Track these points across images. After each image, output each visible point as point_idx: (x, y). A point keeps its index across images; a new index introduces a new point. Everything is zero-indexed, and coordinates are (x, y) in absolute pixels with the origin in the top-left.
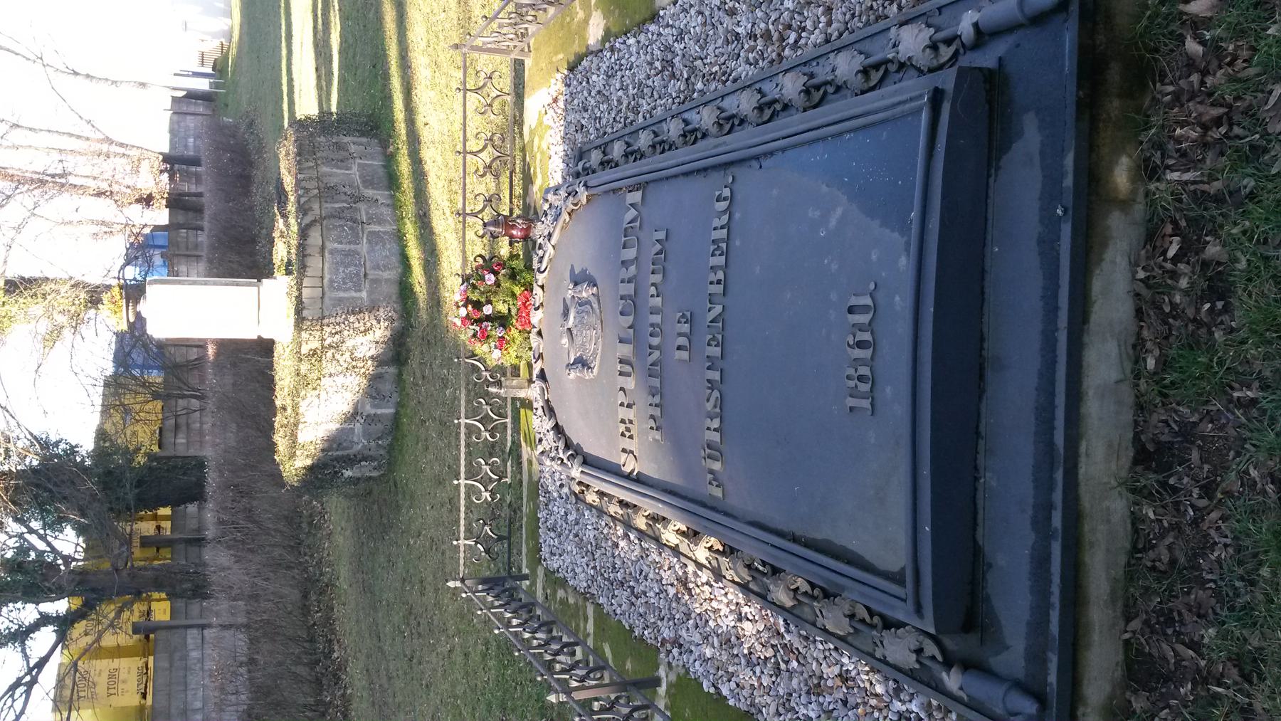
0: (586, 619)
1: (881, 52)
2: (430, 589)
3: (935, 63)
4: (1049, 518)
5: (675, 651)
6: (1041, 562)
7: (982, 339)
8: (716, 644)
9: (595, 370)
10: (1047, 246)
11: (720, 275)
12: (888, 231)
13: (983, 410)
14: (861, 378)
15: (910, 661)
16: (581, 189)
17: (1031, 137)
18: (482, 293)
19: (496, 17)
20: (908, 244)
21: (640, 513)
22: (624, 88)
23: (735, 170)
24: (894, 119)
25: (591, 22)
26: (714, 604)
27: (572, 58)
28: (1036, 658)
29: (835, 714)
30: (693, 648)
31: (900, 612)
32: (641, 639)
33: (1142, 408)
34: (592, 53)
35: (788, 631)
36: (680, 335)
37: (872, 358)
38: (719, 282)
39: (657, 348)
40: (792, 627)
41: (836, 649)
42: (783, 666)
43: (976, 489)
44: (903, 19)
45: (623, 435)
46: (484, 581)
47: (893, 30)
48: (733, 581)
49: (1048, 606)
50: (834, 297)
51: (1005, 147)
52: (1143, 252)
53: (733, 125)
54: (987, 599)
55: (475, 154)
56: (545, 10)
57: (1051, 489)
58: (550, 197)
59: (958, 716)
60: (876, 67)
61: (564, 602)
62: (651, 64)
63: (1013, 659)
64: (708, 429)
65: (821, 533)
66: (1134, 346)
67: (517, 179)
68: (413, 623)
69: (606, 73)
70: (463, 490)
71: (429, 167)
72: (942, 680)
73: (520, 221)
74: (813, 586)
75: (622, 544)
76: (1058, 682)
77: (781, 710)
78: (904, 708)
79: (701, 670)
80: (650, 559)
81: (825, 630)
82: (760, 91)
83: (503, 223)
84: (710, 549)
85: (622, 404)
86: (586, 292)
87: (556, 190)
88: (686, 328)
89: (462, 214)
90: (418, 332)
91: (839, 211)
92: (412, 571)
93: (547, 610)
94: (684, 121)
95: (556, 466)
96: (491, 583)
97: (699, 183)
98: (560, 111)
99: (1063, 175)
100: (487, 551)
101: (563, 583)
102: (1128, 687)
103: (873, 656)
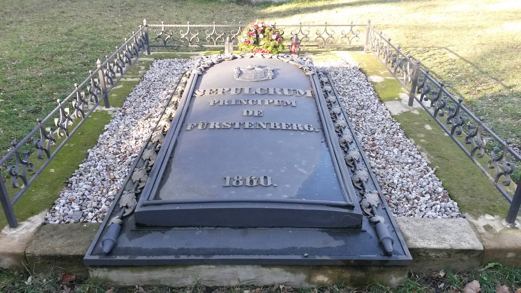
0: (132, 78)
1: (368, 187)
2: (142, 14)
3: (363, 207)
4: (184, 254)
5: (121, 114)
6: (166, 252)
7: (255, 227)
8: (125, 130)
9: (238, 79)
10: (293, 250)
11: (278, 127)
12: (297, 190)
13: (226, 229)
14: (238, 182)
15: (123, 204)
16: (312, 72)
17: (335, 243)
18: (268, 33)
19: (382, 37)
20: (293, 198)
21: (179, 99)
22: (353, 90)
23: (321, 131)
24: (342, 192)
25: (379, 77)
26: (142, 129)
27: (364, 70)
28: (127, 251)
29: (99, 176)
30: (123, 120)
31: (143, 199)
32: (125, 100)
33: (228, 289)
34: (367, 77)
35: (132, 157)
36: (253, 112)
37: (246, 186)
38: (275, 127)
39: (248, 103)
40: (134, 159)
41: (126, 176)
42: (117, 156)
43: (194, 227)
44: (381, 195)
45: (211, 90)
46: (147, 35)
47: (377, 192)
48: (152, 136)
49: (148, 255)
50: (271, 171)
51: (331, 234)
52: (290, 287)
53: (338, 132)
54: (150, 232)
55: (326, 30)
56: (384, 58)
57: (196, 255)
58: (308, 60)
59: (101, 223)
60: (362, 186)
61: (139, 69)
62: (362, 101)
63: (125, 242)
64: (215, 124)
65: (174, 168)
66: (253, 285)
67: (315, 49)
68: (127, 8)
69: (359, 83)
70: (185, 26)
71: (319, 13)
72: (115, 216)
73: (298, 49)
74: (152, 166)
75: (165, 92)
76: (118, 260)
77: (99, 156)
78: (103, 202)
79: (114, 124)
80: (159, 103)
81: (133, 172)
82: (352, 142)
83: (297, 43)
84: (165, 126)
85: (224, 89)
86: (270, 74)
87: (311, 63)
88: (256, 114)
89: (301, 25)
90: (251, 9)
91: (305, 172)
92: (149, 7)
93: (135, 62)
94: (340, 114)
95: (197, 64)
96: (146, 38)
97: (316, 119)
98: (343, 65)
99: (320, 255)
100: (159, 37)
101: (147, 69)
102: (116, 288)
103: (123, 190)
